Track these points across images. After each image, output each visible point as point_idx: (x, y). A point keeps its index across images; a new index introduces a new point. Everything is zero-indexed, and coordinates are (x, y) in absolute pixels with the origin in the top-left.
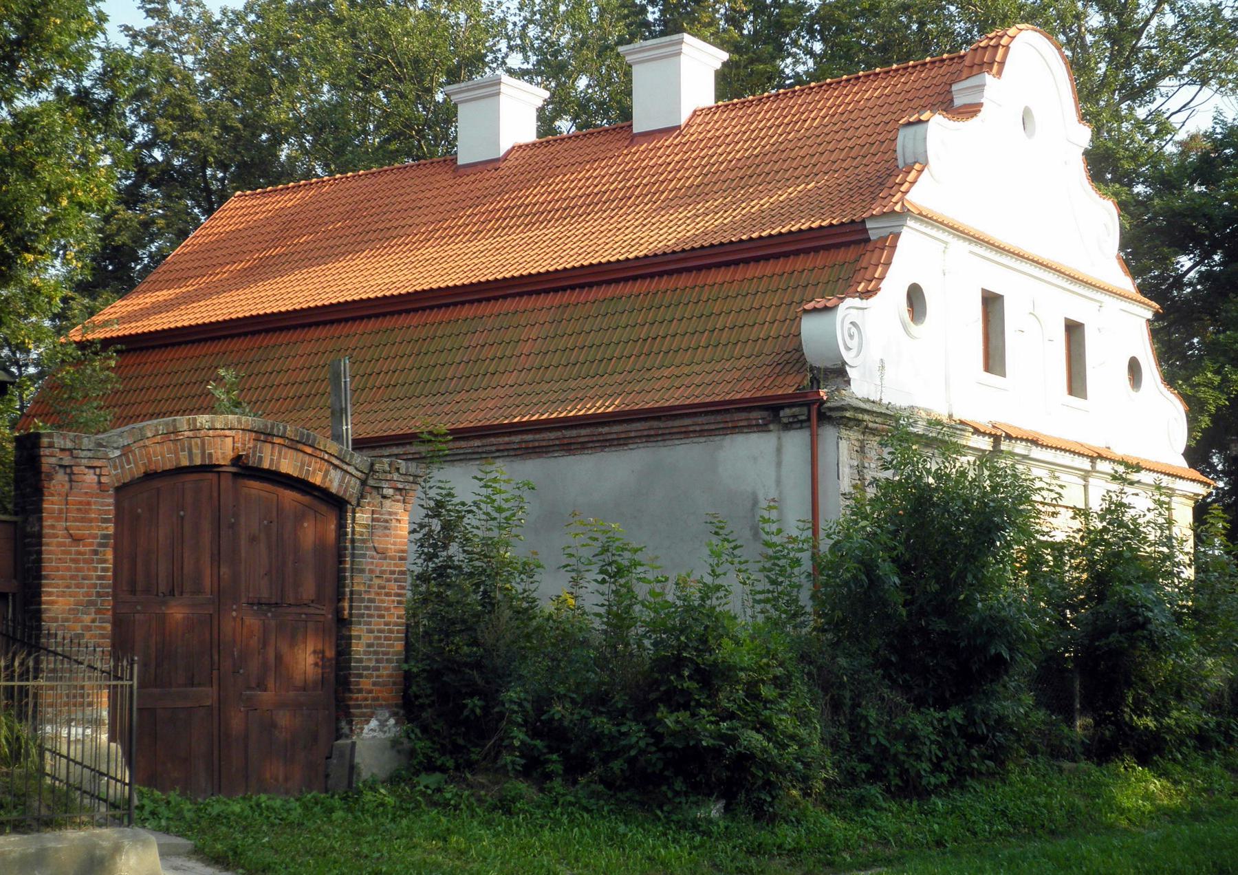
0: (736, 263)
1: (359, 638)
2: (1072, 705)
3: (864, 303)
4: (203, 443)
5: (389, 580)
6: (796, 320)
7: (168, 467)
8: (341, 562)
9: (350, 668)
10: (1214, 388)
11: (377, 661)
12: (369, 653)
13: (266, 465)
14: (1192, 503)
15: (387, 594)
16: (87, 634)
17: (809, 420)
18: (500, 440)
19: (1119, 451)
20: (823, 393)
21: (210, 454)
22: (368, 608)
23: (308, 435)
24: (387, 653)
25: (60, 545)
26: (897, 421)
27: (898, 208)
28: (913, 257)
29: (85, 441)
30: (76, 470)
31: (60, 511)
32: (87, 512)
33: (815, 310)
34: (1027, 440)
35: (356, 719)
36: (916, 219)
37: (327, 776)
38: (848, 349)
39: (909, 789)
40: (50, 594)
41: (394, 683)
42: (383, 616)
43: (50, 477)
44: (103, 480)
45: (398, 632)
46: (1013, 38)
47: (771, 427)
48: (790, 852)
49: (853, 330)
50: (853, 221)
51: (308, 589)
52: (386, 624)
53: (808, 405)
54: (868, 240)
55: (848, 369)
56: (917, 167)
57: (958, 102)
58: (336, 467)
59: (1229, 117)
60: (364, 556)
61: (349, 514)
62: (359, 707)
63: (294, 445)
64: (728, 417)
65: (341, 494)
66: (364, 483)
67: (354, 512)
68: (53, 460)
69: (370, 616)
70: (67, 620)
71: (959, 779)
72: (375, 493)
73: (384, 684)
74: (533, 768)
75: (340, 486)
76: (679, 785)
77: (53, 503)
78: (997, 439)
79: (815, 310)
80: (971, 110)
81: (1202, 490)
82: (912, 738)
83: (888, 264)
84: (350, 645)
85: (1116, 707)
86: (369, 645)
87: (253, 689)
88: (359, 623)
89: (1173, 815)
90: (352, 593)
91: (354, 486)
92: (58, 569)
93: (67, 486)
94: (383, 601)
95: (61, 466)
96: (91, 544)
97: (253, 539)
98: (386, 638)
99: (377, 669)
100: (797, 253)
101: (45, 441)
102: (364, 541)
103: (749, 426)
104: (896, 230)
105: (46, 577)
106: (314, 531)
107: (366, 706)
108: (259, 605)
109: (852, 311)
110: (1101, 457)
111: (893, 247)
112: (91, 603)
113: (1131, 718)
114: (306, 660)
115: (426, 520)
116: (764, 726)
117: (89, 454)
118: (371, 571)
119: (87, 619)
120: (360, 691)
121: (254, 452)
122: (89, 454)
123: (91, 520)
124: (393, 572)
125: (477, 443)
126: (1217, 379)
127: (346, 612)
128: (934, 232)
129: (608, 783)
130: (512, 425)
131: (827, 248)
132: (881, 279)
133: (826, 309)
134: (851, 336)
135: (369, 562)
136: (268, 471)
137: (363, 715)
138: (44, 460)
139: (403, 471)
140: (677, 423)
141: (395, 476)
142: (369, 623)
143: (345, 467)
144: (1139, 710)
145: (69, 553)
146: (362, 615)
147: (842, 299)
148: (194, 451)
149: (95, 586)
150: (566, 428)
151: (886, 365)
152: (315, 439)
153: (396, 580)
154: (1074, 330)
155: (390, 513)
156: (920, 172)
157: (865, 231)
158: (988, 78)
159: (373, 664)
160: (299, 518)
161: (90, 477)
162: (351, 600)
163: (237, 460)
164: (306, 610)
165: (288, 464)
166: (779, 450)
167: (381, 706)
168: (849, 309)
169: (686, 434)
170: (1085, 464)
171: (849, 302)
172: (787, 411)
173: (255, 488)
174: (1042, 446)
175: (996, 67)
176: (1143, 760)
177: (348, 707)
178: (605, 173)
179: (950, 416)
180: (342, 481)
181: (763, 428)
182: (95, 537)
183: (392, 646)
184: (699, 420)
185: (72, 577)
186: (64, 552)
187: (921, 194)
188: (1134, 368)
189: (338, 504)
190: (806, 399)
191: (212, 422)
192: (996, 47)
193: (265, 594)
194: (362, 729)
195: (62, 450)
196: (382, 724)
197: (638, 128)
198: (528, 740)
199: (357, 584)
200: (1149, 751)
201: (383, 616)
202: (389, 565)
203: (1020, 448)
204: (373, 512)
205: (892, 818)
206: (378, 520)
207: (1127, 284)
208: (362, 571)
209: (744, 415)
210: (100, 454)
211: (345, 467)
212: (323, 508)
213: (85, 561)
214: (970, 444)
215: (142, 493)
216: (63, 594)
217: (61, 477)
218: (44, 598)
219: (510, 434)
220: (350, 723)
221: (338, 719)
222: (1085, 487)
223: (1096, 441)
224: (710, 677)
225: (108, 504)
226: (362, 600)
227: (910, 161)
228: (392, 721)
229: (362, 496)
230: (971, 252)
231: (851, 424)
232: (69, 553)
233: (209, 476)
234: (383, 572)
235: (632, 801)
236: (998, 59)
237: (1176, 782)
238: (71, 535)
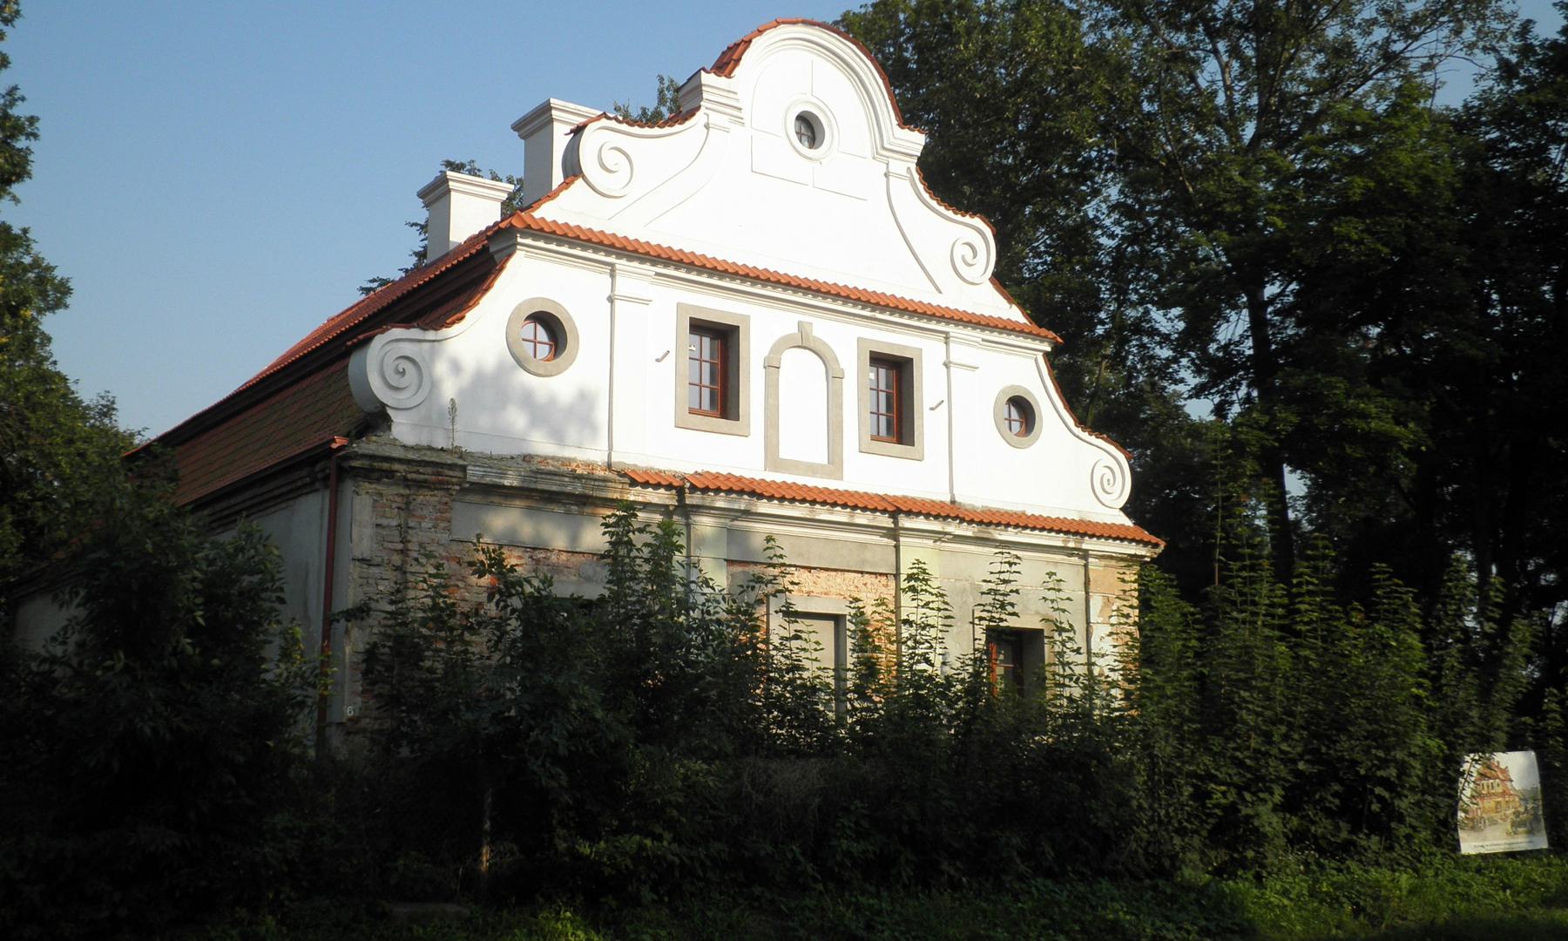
10: (1261, 429)
26: (464, 468)
55: (390, 412)
59: (6, 202)
78: (680, 491)
109: (402, 345)
126: (1265, 419)
128: (933, 325)
170: (886, 521)
188: (1022, 410)
222: (897, 548)
230: (657, 274)
231: (376, 475)
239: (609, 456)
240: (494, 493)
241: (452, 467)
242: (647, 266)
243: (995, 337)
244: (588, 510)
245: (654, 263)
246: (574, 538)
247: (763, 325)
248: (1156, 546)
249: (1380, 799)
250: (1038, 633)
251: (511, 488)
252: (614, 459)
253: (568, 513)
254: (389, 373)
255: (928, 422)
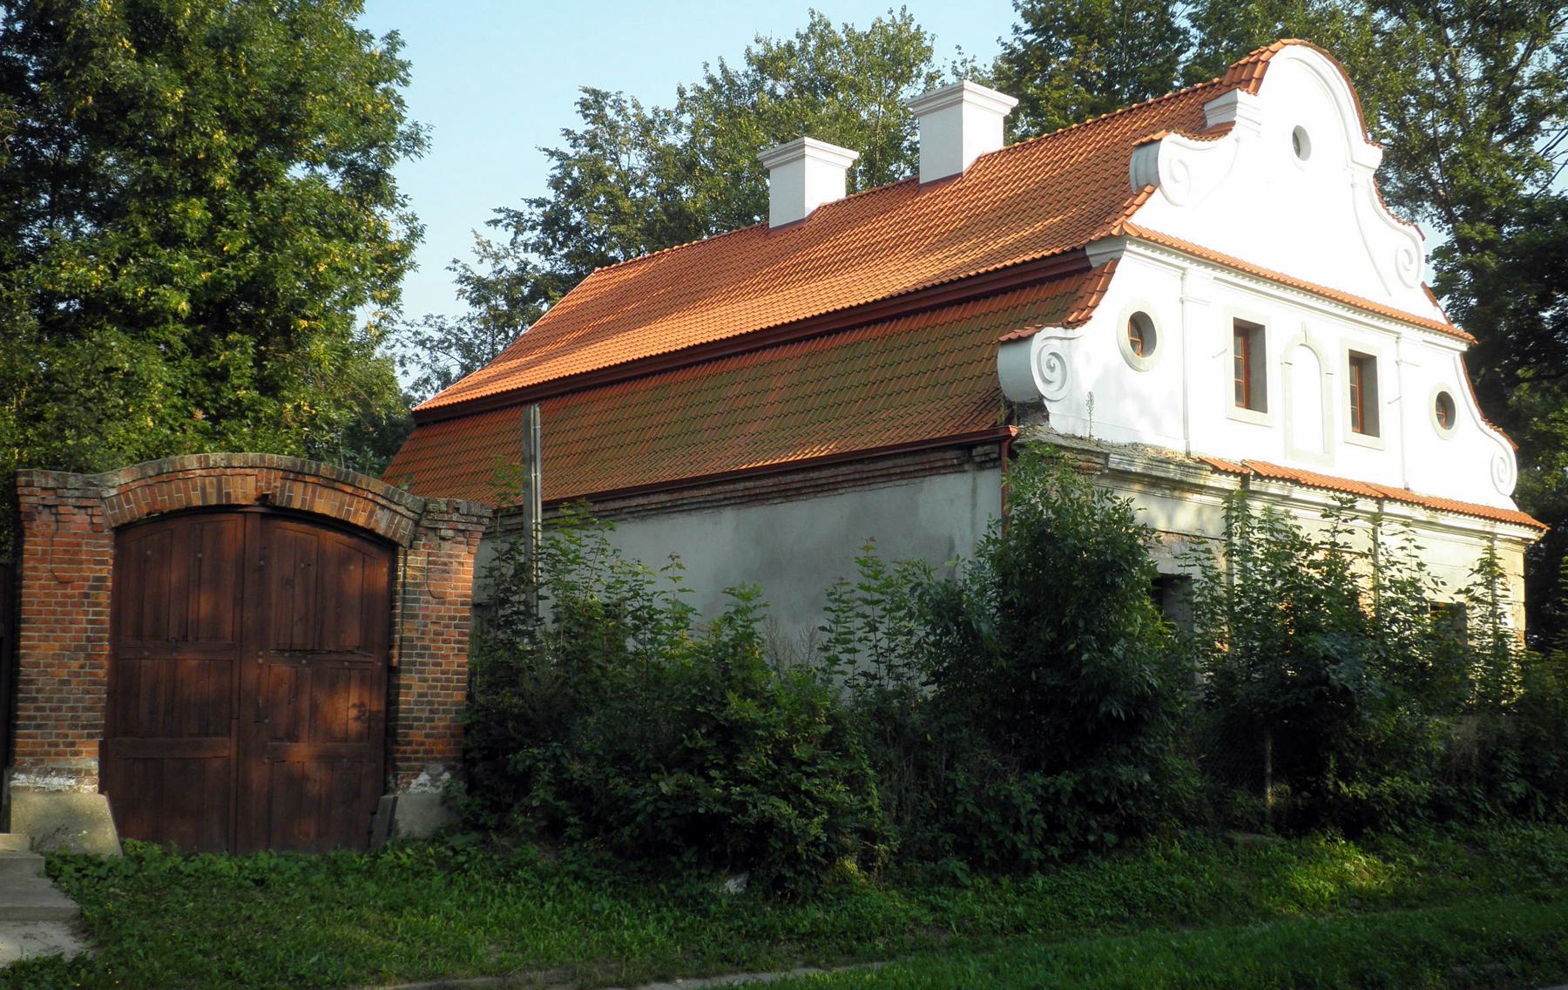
0: (967, 300)
1: (409, 687)
2: (1263, 770)
3: (1070, 333)
4: (219, 483)
5: (447, 626)
6: (993, 357)
7: (177, 506)
8: (393, 607)
9: (397, 719)
11: (431, 711)
12: (422, 703)
13: (296, 505)
14: (1522, 549)
15: (445, 641)
16: (74, 680)
17: (999, 458)
18: (727, 488)
19: (1421, 490)
20: (1014, 430)
21: (228, 494)
22: (422, 656)
23: (347, 474)
24: (445, 704)
25: (43, 587)
26: (1106, 456)
27: (1115, 232)
28: (1134, 281)
29: (72, 480)
30: (62, 509)
31: (45, 553)
32: (76, 553)
33: (1010, 341)
34: (1283, 479)
35: (401, 774)
36: (1139, 244)
37: (370, 833)
38: (1047, 382)
39: (1011, 863)
40: (29, 638)
41: (452, 735)
42: (440, 665)
43: (31, 517)
44: (95, 520)
45: (458, 681)
46: (1274, 53)
47: (966, 467)
48: (802, 938)
49: (1054, 361)
50: (1074, 249)
51: (352, 635)
52: (443, 673)
53: (999, 441)
54: (1089, 268)
56: (1148, 189)
57: (1211, 122)
58: (383, 507)
60: (417, 601)
61: (401, 557)
62: (408, 760)
63: (331, 484)
64: (924, 458)
65: (390, 535)
66: (417, 523)
67: (406, 555)
68: (33, 500)
69: (422, 664)
70: (51, 666)
71: (1077, 853)
72: (431, 534)
73: (441, 736)
74: (553, 830)
75: (389, 527)
76: (690, 856)
77: (35, 544)
78: (1245, 479)
79: (1010, 341)
80: (1224, 129)
81: (1533, 535)
82: (1007, 806)
83: (1104, 291)
84: (398, 695)
85: (1320, 769)
86: (421, 695)
87: (281, 739)
88: (410, 671)
89: (1366, 900)
90: (402, 639)
91: (404, 529)
92: (40, 613)
93: (53, 526)
94: (440, 649)
95: (45, 506)
96: (82, 587)
97: (287, 582)
98: (443, 688)
99: (432, 720)
100: (1023, 286)
101: (22, 479)
102: (416, 585)
103: (944, 467)
104: (1115, 255)
105: (27, 621)
106: (360, 577)
107: (416, 760)
108: (290, 651)
109: (1054, 342)
110: (1386, 497)
111: (1112, 273)
112: (79, 648)
113: (1336, 784)
114: (347, 709)
115: (497, 563)
116: (790, 793)
117: (77, 493)
118: (425, 617)
119: (74, 665)
120: (410, 743)
121: (282, 491)
122: (77, 493)
123: (81, 562)
124: (454, 618)
125: (707, 491)
127: (395, 660)
128: (1172, 260)
129: (619, 851)
130: (739, 471)
131: (1051, 279)
132: (1094, 307)
133: (1021, 340)
134: (1052, 369)
135: (426, 607)
136: (299, 511)
137: (412, 768)
138: (22, 499)
139: (464, 510)
140: (880, 465)
141: (455, 517)
142: (422, 672)
143: (393, 507)
144: (1346, 774)
145: (55, 596)
146: (414, 663)
147: (1039, 329)
148: (209, 490)
149: (85, 630)
150: (780, 474)
151: (1095, 399)
152: (355, 478)
153: (456, 627)
154: (1362, 364)
155: (450, 556)
156: (1150, 194)
157: (1086, 258)
158: (1241, 95)
159: (426, 714)
160: (344, 561)
161: (81, 518)
162: (401, 647)
163: (263, 499)
164: (349, 657)
165: (324, 505)
166: (974, 491)
167: (436, 760)
168: (1047, 340)
169: (888, 477)
171: (1049, 331)
172: (980, 450)
173: (291, 529)
174: (1306, 485)
175: (1253, 83)
176: (1353, 833)
177: (395, 760)
178: (882, 227)
179: (1188, 454)
180: (391, 521)
181: (958, 469)
182: (86, 579)
183: (451, 696)
184: (899, 461)
185: (57, 621)
186: (47, 595)
187: (1148, 216)
188: (1445, 406)
189: (389, 547)
190: (998, 432)
191: (229, 459)
192: (1255, 63)
193: (298, 641)
194: (409, 784)
195: (44, 489)
196: (435, 779)
197: (924, 178)
198: (550, 798)
199: (406, 630)
200: (1359, 824)
201: (440, 665)
202: (448, 610)
203: (1274, 488)
204: (429, 555)
205: (980, 899)
206: (434, 563)
207: (1436, 312)
208: (414, 616)
209: (939, 455)
210: (90, 494)
211: (393, 507)
212: (373, 550)
213: (73, 605)
214: (1210, 483)
215: (134, 537)
216: (46, 639)
217: (46, 516)
218: (23, 643)
219: (734, 481)
220: (395, 777)
221: (386, 772)
223: (1390, 480)
224: (732, 736)
225: (106, 547)
226: (415, 647)
227: (1142, 184)
228: (447, 776)
229: (416, 538)
232: (55, 596)
233: (234, 516)
234: (442, 618)
235: (641, 871)
236: (1256, 75)
237: (1387, 859)
238: (56, 578)
239: (1188, 443)
240: (1124, 477)
241: (1097, 454)
242: (1209, 270)
243: (1231, 277)
244: (1177, 494)
245: (1214, 268)
246: (1170, 519)
247: (1283, 324)
248: (1541, 530)
249: (599, 667)
250: (1460, 607)
251: (1136, 474)
252: (1192, 450)
253: (1164, 497)
254: (1044, 368)
255: (1387, 413)
